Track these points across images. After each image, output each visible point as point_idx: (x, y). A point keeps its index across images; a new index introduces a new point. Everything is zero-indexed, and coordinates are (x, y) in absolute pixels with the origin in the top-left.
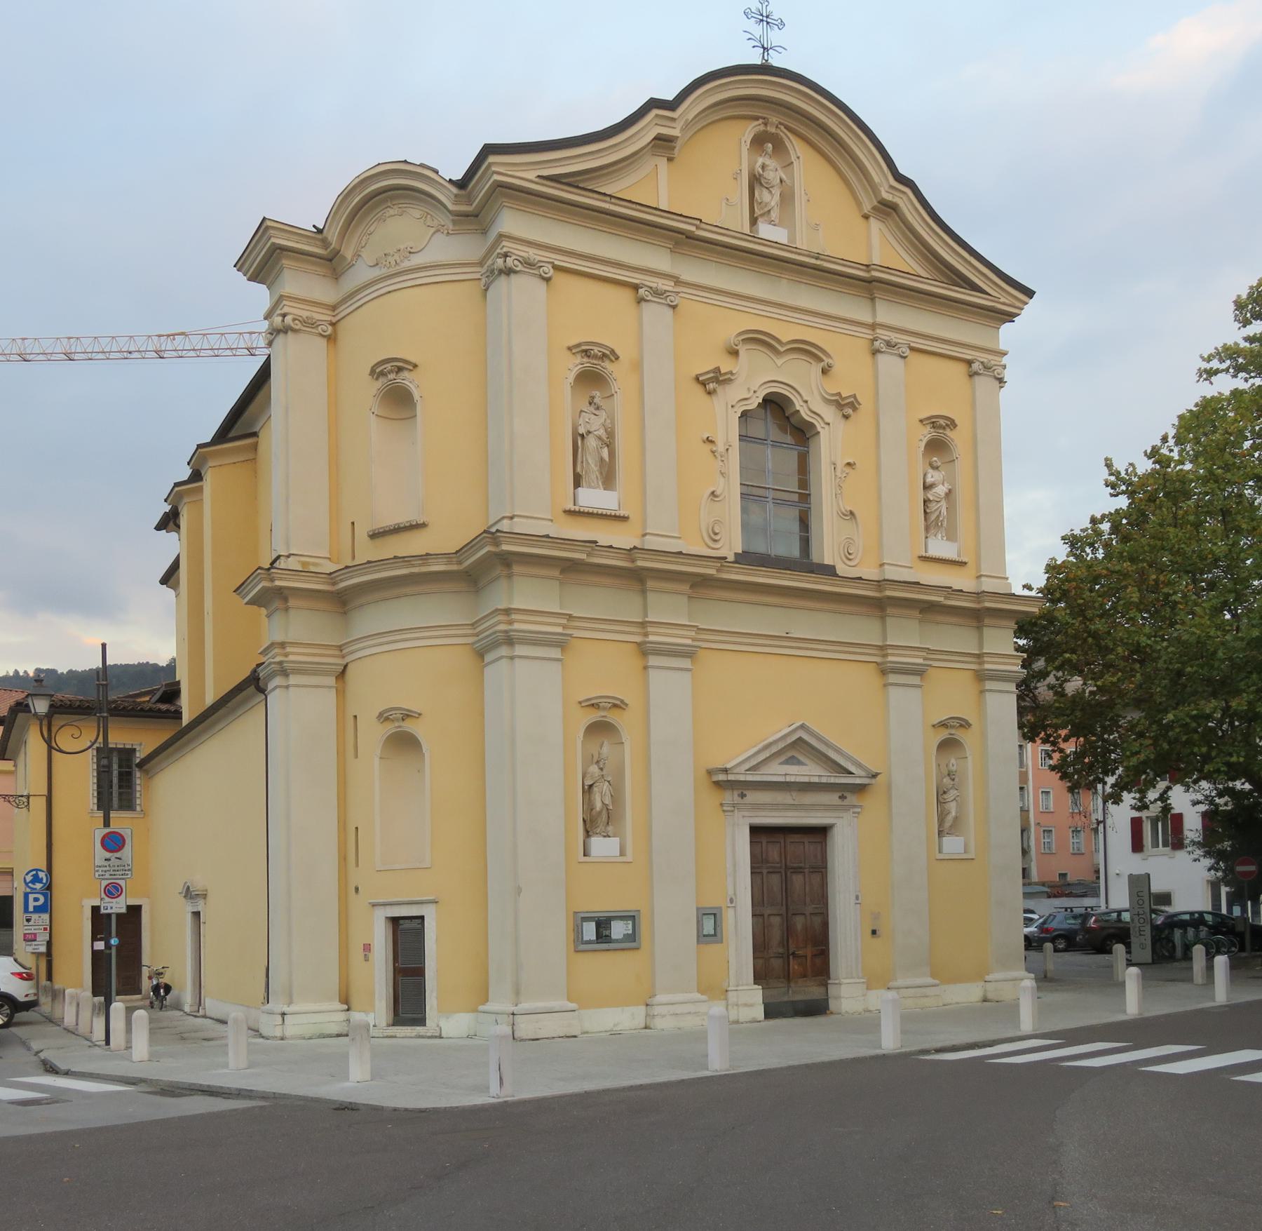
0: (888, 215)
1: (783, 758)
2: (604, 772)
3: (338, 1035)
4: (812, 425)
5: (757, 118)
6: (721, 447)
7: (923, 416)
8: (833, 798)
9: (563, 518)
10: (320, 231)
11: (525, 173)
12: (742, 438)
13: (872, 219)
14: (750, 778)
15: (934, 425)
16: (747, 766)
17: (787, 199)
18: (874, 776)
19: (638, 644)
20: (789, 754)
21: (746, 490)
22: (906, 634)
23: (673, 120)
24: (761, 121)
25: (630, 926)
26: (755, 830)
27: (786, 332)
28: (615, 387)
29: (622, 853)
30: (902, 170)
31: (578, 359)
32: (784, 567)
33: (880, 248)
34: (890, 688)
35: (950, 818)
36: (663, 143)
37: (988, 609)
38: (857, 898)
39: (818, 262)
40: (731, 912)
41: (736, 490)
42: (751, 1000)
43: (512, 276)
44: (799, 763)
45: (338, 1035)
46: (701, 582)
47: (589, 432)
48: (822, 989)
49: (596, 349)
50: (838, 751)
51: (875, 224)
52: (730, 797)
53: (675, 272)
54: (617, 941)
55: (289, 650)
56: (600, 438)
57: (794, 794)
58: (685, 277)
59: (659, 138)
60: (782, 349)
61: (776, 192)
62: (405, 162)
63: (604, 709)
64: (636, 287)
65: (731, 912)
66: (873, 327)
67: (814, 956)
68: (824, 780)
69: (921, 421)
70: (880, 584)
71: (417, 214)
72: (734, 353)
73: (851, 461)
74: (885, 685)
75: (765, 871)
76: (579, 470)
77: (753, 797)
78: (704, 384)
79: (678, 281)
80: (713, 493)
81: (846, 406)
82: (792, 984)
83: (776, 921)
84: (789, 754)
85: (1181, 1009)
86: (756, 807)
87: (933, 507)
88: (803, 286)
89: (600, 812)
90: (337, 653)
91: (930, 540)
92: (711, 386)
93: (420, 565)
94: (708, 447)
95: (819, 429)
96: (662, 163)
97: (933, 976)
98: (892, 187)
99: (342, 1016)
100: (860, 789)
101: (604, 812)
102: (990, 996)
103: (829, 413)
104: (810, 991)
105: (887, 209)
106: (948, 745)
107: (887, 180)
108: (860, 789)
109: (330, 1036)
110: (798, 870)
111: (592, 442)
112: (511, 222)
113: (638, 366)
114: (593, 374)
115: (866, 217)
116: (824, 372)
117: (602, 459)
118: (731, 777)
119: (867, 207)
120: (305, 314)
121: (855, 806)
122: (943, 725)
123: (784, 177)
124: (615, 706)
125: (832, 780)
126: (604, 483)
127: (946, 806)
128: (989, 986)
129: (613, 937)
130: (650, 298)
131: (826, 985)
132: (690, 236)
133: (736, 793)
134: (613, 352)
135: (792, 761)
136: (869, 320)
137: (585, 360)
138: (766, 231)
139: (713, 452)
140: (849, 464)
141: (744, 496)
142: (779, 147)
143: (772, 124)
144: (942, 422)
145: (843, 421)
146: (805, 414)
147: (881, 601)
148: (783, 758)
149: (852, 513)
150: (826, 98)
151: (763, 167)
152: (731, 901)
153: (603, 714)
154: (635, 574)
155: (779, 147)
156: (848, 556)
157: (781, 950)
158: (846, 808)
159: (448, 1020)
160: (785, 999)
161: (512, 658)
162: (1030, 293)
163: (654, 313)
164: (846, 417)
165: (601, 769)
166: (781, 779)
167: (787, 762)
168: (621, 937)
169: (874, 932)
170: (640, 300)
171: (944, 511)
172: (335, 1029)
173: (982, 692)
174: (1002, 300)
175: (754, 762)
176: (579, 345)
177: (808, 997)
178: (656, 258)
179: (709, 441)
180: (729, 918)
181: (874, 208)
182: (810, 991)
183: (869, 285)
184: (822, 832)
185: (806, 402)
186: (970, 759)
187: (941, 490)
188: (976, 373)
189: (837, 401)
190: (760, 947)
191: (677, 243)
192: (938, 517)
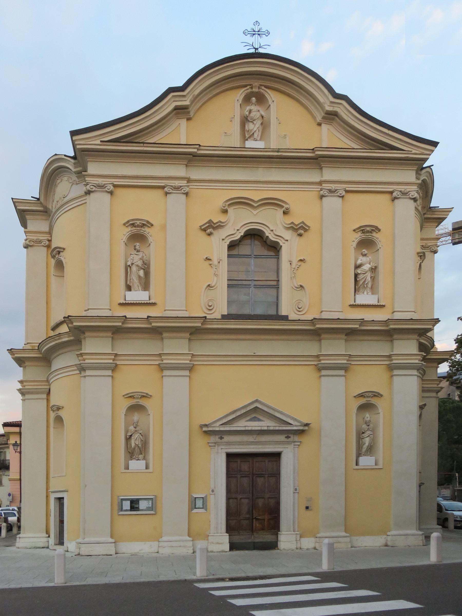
0: (333, 119)
1: (248, 418)
2: (137, 429)
3: (43, 548)
4: (278, 243)
5: (246, 86)
6: (215, 261)
7: (355, 227)
8: (282, 438)
9: (118, 307)
10: (38, 199)
11: (93, 141)
12: (229, 256)
13: (323, 125)
14: (222, 429)
15: (363, 232)
16: (221, 422)
17: (265, 126)
18: (307, 425)
19: (159, 365)
20: (253, 416)
21: (231, 283)
22: (334, 348)
23: (184, 96)
24: (248, 87)
25: (150, 503)
26: (230, 456)
27: (256, 196)
28: (150, 239)
29: (147, 468)
30: (338, 90)
31: (130, 229)
32: (255, 320)
33: (329, 138)
34: (323, 378)
35: (365, 447)
36: (181, 111)
37: (395, 329)
38: (296, 490)
39: (279, 154)
40: (212, 497)
41: (225, 283)
42: (221, 541)
43: (92, 194)
44: (259, 420)
45: (43, 548)
46: (197, 330)
47: (132, 264)
48: (274, 537)
49: (138, 222)
50: (281, 413)
51: (325, 127)
52: (215, 439)
53: (188, 176)
54: (142, 510)
55: (25, 384)
56: (137, 266)
57: (255, 436)
58: (193, 177)
59: (177, 108)
60: (256, 205)
61: (258, 123)
62: (56, 155)
63: (137, 398)
64: (163, 187)
65: (212, 497)
66: (320, 183)
67: (269, 519)
68: (277, 428)
69: (354, 230)
70: (313, 321)
71: (58, 181)
72: (225, 212)
73: (302, 258)
74: (320, 376)
75: (239, 476)
76: (128, 283)
77: (227, 438)
78: (205, 230)
79: (189, 180)
80: (209, 285)
81: (300, 229)
82: (255, 534)
83: (245, 501)
84: (253, 416)
85: (379, 566)
86: (229, 444)
87: (361, 277)
88: (273, 169)
89: (134, 449)
90: (48, 384)
91: (357, 296)
92: (209, 231)
93: (59, 339)
94: (208, 262)
95: (281, 244)
96: (183, 122)
97: (346, 531)
98: (332, 102)
99: (46, 540)
100: (301, 432)
101: (137, 448)
102: (389, 543)
103: (287, 235)
104: (267, 537)
105: (331, 117)
106: (365, 407)
107: (328, 98)
108: (301, 432)
109: (39, 548)
110: (260, 476)
111: (134, 268)
112: (93, 168)
113: (164, 227)
114: (138, 234)
115: (319, 124)
116: (285, 213)
117: (139, 277)
118: (210, 429)
119: (319, 119)
120: (35, 238)
121: (295, 442)
122: (361, 395)
123: (263, 113)
124: (144, 396)
125: (280, 428)
126: (144, 288)
127: (363, 440)
128: (389, 538)
129: (140, 508)
130: (171, 191)
131: (277, 535)
132: (194, 155)
133: (217, 437)
134: (148, 222)
135: (255, 419)
136: (318, 180)
137: (134, 228)
138: (250, 144)
139: (210, 265)
140: (301, 260)
141: (229, 286)
142: (261, 99)
143: (256, 86)
144: (368, 229)
145: (298, 237)
146: (272, 237)
147: (316, 331)
148: (248, 418)
149: (301, 286)
150: (290, 64)
151: (250, 111)
152: (213, 491)
153: (137, 400)
154: (155, 330)
155: (261, 99)
156: (299, 309)
157: (248, 516)
158: (289, 443)
159: (70, 545)
160: (250, 541)
161: (85, 377)
162: (435, 144)
163: (176, 200)
164: (300, 235)
165: (135, 428)
166: (243, 429)
167: (251, 420)
168: (145, 508)
169: (307, 508)
170: (167, 194)
171: (369, 278)
172: (41, 545)
173: (392, 376)
174: (414, 151)
175: (225, 421)
176: (128, 222)
177: (265, 540)
178: (178, 170)
179: (207, 259)
180: (211, 500)
181: (324, 118)
182: (267, 537)
183: (316, 160)
184: (277, 456)
185: (272, 231)
186: (381, 414)
187: (367, 267)
188: (396, 198)
189: (292, 227)
190: (230, 514)
191: (190, 161)
192: (364, 282)
